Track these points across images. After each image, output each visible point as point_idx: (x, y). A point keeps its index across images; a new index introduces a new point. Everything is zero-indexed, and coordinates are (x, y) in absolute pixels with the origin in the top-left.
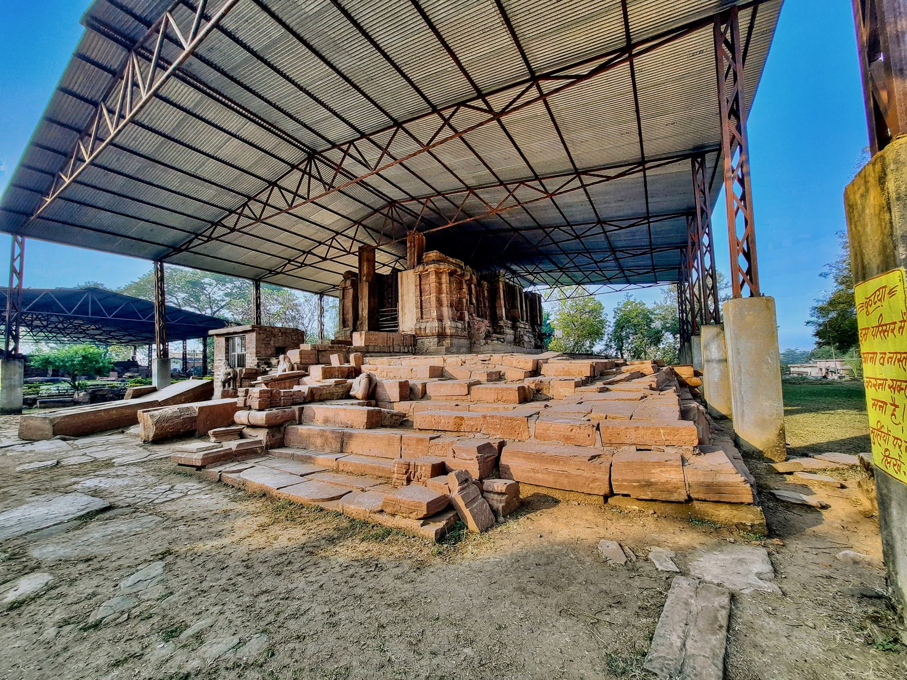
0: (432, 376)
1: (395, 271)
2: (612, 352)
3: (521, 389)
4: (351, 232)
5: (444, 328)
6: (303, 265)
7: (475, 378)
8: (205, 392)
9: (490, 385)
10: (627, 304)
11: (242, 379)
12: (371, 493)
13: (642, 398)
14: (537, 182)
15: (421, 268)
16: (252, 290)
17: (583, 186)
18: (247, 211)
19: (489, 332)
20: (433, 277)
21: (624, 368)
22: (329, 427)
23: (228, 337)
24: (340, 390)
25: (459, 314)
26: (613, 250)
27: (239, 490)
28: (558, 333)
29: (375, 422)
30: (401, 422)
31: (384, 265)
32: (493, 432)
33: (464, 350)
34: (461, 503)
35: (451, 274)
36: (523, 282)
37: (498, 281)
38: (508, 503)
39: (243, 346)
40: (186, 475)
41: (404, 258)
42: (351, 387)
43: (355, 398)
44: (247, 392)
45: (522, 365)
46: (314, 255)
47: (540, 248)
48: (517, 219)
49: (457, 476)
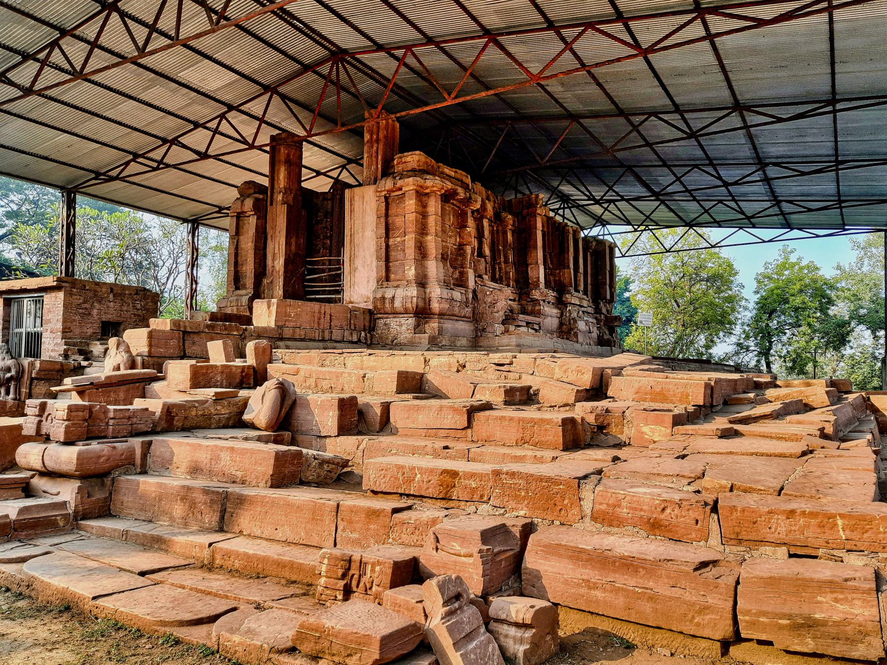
0: (401, 390)
2: (750, 359)
3: (569, 424)
4: (256, 107)
5: (427, 301)
6: (161, 165)
7: (483, 397)
9: (510, 412)
10: (783, 267)
11: (32, 379)
12: (276, 613)
13: (804, 454)
14: (619, 26)
15: (388, 184)
17: (710, 37)
18: (56, 57)
19: (511, 311)
20: (411, 203)
21: (770, 393)
22: (200, 483)
24: (224, 411)
25: (457, 275)
26: (761, 163)
27: (20, 596)
28: (644, 317)
29: (288, 474)
30: (340, 476)
31: (318, 173)
32: (512, 504)
33: (464, 342)
34: (445, 641)
35: (447, 197)
36: (582, 219)
37: (534, 215)
38: (535, 644)
39: (39, 316)
41: (358, 162)
44: (43, 407)
46: (184, 146)
47: (620, 155)
48: (578, 95)
49: (442, 587)
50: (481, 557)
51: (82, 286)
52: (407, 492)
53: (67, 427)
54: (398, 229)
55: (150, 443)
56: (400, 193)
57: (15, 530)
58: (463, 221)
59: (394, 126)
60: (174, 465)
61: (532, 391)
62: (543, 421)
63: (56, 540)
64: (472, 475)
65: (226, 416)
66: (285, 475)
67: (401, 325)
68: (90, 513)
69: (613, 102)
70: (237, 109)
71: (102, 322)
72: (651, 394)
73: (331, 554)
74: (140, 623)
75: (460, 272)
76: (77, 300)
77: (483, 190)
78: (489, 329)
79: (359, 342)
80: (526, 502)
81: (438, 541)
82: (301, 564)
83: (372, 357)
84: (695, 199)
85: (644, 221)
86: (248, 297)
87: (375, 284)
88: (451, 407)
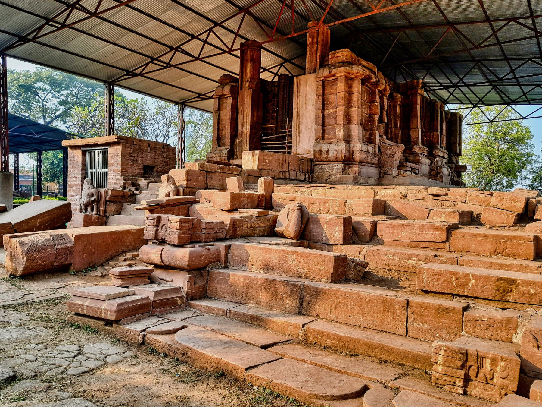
4: (233, 24)
5: (351, 152)
6: (168, 65)
8: (59, 218)
15: (325, 72)
20: (341, 85)
23: (86, 150)
24: (262, 225)
25: (368, 135)
33: (372, 181)
35: (365, 81)
37: (416, 94)
40: (89, 330)
43: (281, 235)
45: (506, 205)
52: (460, 293)
53: (179, 234)
54: (331, 103)
56: (334, 78)
57: (154, 308)
58: (372, 98)
59: (327, 33)
60: (250, 263)
64: (530, 283)
65: (264, 228)
67: (333, 169)
69: (485, 12)
70: (220, 25)
71: (144, 166)
73: (447, 347)
81: (537, 341)
82: (392, 348)
83: (332, 190)
84: (519, 85)
86: (226, 151)
87: (314, 141)
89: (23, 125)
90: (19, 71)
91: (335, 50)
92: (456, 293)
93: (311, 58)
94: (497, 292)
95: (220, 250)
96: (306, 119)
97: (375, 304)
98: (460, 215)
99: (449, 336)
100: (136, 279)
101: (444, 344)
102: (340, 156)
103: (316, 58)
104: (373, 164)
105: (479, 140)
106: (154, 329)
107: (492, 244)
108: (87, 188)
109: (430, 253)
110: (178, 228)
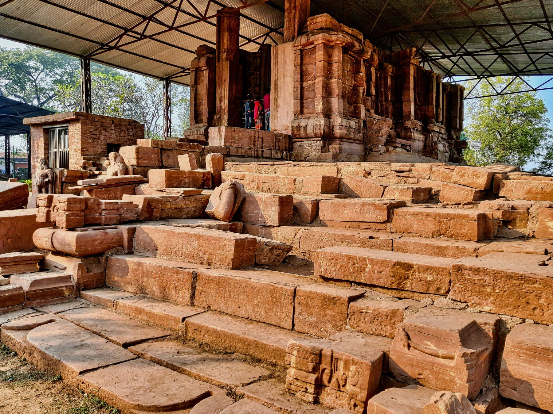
0: (325, 190)
1: (265, 49)
5: (331, 128)
6: (143, 36)
7: (398, 198)
9: (421, 208)
11: (63, 183)
15: (303, 40)
16: (80, 71)
20: (320, 54)
24: (192, 205)
25: (352, 109)
29: (247, 258)
30: (283, 260)
31: (250, 40)
32: (475, 299)
35: (347, 49)
37: (408, 64)
42: (207, 201)
45: (468, 180)
50: (466, 361)
51: (94, 118)
52: (357, 280)
53: (67, 216)
54: (309, 74)
55: (134, 230)
56: (312, 46)
57: (28, 299)
61: (433, 192)
62: (458, 216)
63: (60, 308)
64: (428, 269)
65: (193, 209)
66: (243, 259)
67: (312, 147)
68: (89, 285)
71: (108, 144)
72: (542, 194)
73: (300, 347)
74: (120, 404)
75: (354, 107)
76: (90, 128)
77: (371, 45)
78: (375, 149)
79: (281, 159)
80: (492, 298)
81: (409, 338)
82: (265, 345)
83: (296, 168)
85: (484, 72)
86: (204, 128)
87: (293, 116)
88: (372, 204)
89: (7, 105)
90: (8, 49)
91: (314, 15)
92: (353, 280)
93: (290, 26)
94: (394, 279)
95: (122, 233)
96: (285, 92)
97: (264, 293)
98: (413, 192)
99: (333, 330)
100: (21, 266)
101: (298, 343)
102: (319, 132)
103: (294, 24)
104: (357, 140)
105: (490, 114)
106: (11, 324)
107: (434, 224)
108: (40, 168)
109: (365, 234)
110: (66, 208)
